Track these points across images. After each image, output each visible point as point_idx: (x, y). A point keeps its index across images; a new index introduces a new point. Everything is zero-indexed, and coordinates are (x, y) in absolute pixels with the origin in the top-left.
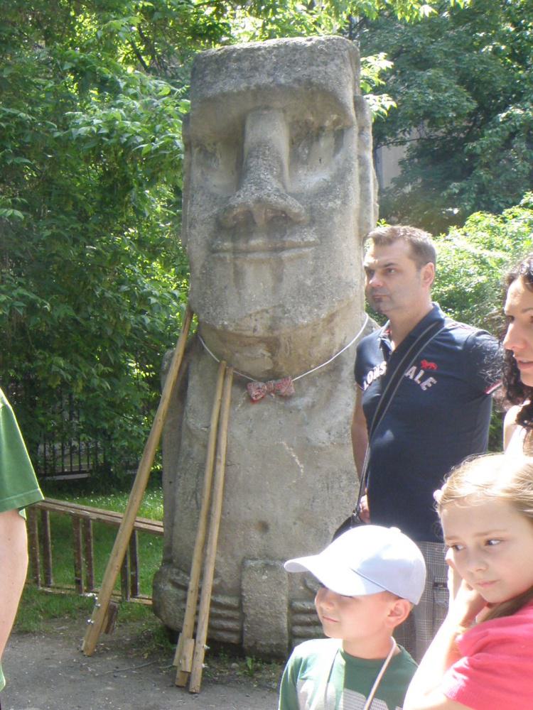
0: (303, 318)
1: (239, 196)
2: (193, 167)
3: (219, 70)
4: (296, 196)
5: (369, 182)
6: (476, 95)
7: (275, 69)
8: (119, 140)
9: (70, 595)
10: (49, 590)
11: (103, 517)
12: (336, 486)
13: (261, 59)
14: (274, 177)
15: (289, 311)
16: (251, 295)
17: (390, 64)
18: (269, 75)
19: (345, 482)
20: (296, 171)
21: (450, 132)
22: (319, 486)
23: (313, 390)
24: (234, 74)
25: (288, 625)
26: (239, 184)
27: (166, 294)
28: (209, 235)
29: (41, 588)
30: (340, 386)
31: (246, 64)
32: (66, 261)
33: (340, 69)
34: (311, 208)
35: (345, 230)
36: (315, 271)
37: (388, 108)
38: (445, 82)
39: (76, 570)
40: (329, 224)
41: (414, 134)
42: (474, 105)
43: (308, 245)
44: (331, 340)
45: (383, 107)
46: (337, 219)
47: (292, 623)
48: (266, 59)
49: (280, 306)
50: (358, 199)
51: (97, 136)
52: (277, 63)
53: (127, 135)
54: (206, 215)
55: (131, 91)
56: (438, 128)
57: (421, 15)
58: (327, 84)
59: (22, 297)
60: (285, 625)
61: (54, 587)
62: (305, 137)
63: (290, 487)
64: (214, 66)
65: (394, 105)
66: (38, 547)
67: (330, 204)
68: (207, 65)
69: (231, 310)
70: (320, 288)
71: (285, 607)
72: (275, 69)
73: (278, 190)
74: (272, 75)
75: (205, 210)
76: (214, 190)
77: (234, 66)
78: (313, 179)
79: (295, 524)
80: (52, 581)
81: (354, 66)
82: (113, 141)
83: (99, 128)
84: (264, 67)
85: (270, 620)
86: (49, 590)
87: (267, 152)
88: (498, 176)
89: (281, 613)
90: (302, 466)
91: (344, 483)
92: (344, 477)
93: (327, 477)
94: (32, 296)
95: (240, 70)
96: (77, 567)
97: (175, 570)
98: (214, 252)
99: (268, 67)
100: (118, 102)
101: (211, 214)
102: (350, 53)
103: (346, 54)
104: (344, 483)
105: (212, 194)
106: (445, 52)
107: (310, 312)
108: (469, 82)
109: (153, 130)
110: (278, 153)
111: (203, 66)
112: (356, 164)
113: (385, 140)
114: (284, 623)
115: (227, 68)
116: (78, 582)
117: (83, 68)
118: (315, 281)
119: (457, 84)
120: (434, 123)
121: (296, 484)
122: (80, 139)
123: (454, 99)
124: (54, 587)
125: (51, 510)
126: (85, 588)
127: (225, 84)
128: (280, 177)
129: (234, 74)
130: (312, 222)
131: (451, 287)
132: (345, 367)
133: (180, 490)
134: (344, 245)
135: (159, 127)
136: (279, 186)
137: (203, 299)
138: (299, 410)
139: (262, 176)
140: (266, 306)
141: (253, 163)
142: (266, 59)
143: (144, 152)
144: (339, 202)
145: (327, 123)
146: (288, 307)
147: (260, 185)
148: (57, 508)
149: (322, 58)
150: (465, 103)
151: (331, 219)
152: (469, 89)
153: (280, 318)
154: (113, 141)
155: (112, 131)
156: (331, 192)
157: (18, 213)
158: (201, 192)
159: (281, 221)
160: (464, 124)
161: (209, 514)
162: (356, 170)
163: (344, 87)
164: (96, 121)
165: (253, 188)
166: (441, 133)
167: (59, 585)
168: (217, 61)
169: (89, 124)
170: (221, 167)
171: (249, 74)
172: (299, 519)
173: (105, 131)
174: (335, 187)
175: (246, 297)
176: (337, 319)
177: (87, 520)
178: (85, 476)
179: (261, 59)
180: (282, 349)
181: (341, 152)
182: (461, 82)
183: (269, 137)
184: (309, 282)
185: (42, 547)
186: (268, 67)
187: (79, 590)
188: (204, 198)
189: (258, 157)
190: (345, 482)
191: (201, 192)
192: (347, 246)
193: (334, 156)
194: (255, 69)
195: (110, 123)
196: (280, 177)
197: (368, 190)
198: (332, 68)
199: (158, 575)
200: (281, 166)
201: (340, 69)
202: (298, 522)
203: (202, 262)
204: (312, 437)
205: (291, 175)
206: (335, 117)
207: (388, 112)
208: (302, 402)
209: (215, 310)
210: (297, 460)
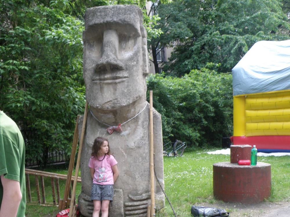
0: (124, 103)
1: (101, 60)
2: (86, 50)
3: (94, 15)
4: (121, 61)
5: (146, 56)
6: (193, 32)
7: (113, 15)
8: (61, 41)
9: (51, 206)
10: (44, 205)
11: (61, 177)
12: (138, 161)
13: (108, 12)
14: (113, 54)
15: (119, 101)
16: (106, 96)
17: (160, 18)
18: (111, 18)
19: (140, 160)
20: (121, 52)
21: (186, 44)
22: (132, 162)
23: (129, 128)
24: (99, 17)
25: (124, 211)
26: (101, 56)
27: (82, 97)
28: (92, 74)
29: (41, 205)
30: (138, 127)
31: (103, 14)
32: (46, 85)
33: (135, 16)
34: (126, 65)
35: (138, 72)
36: (128, 86)
37: (161, 34)
38: (183, 26)
39: (53, 197)
40: (132, 70)
41: (175, 43)
42: (192, 34)
43: (125, 77)
44: (135, 111)
45: (159, 33)
46: (135, 68)
47: (125, 211)
48: (110, 12)
49: (116, 99)
50: (142, 62)
51: (54, 39)
52: (113, 13)
53: (64, 39)
54: (90, 67)
55: (68, 23)
56: (183, 42)
57: (169, 2)
58: (130, 21)
59: (28, 99)
60: (123, 211)
61: (46, 204)
62: (123, 39)
63: (122, 163)
64: (92, 14)
65: (163, 33)
66: (39, 189)
67: (132, 63)
68: (90, 14)
69: (99, 101)
70: (129, 93)
71: (123, 205)
72: (113, 15)
73: (114, 58)
74: (112, 18)
75: (90, 65)
76: (93, 58)
77: (99, 14)
78: (127, 54)
79: (124, 175)
80: (45, 202)
81: (140, 16)
82: (59, 41)
83: (54, 37)
84: (109, 15)
85: (117, 210)
86: (44, 205)
87: (111, 45)
88: (199, 58)
89: (121, 207)
90: (126, 155)
91: (140, 160)
92: (140, 158)
93: (134, 159)
94: (33, 99)
95: (101, 15)
96: (54, 196)
97: (84, 195)
98: (93, 80)
99: (110, 15)
100: (63, 27)
101: (92, 67)
102: (138, 11)
103: (137, 11)
104: (140, 160)
105: (92, 60)
106: (183, 17)
107: (126, 101)
108: (191, 27)
109: (74, 37)
110: (114, 45)
111: (88, 14)
112: (141, 49)
113: (166, 45)
114: (122, 210)
115: (96, 15)
116: (54, 202)
117: (51, 15)
118: (128, 90)
119: (187, 27)
120: (181, 40)
121: (124, 162)
122: (48, 40)
123: (186, 32)
124: (46, 204)
125: (44, 176)
126: (57, 203)
127: (96, 20)
128: (115, 54)
129: (99, 17)
130: (127, 69)
131: (185, 94)
132: (140, 120)
133: (85, 166)
134: (137, 78)
135: (76, 36)
136: (115, 57)
137: (90, 97)
138: (125, 136)
139: (109, 54)
140: (111, 99)
141: (106, 49)
142: (110, 12)
143: (70, 45)
144: (135, 63)
145: (131, 35)
146: (119, 99)
147: (108, 56)
148: (45, 175)
149: (129, 12)
150: (189, 34)
151: (133, 68)
152: (191, 29)
153: (116, 103)
154: (59, 41)
155: (59, 37)
156: (133, 59)
157: (26, 68)
158: (89, 59)
159: (115, 68)
160: (191, 41)
161: (40, 173)
162: (141, 52)
163: (136, 23)
164: (53, 34)
165: (106, 57)
166: (184, 43)
167: (48, 203)
168: (93, 12)
169: (51, 34)
170: (96, 50)
171: (104, 17)
172: (125, 173)
173: (56, 37)
174: (134, 57)
175: (104, 96)
176: (136, 104)
177: (56, 179)
178: (64, 163)
179: (108, 12)
180: (118, 115)
181: (136, 45)
182: (188, 27)
183: (111, 40)
184: (126, 91)
185: (41, 189)
186: (110, 15)
187: (55, 204)
188: (90, 61)
189: (107, 47)
190: (140, 160)
191: (89, 59)
192: (139, 78)
193: (134, 46)
194: (106, 15)
195: (59, 35)
196: (115, 54)
197: (145, 59)
198: (132, 16)
199: (79, 197)
200: (116, 50)
201: (135, 16)
202: (126, 175)
203: (89, 84)
204: (129, 145)
205: (119, 53)
206: (134, 33)
207: (160, 35)
208: (124, 133)
209: (94, 101)
210: (124, 153)
